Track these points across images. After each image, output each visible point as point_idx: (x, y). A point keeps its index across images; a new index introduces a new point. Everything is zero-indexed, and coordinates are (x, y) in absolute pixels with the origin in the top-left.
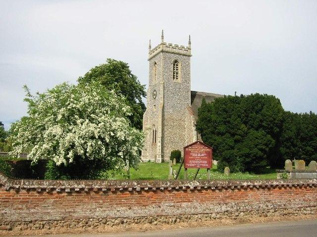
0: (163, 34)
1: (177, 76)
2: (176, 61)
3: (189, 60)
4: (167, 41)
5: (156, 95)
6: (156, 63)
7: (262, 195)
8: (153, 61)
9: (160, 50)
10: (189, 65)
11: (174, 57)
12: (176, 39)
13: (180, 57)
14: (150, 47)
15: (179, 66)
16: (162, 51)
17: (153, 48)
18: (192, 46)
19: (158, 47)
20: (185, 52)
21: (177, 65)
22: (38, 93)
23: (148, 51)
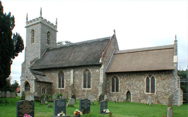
2: (48, 32)
8: (31, 28)
16: (41, 23)
19: (37, 19)
20: (54, 28)
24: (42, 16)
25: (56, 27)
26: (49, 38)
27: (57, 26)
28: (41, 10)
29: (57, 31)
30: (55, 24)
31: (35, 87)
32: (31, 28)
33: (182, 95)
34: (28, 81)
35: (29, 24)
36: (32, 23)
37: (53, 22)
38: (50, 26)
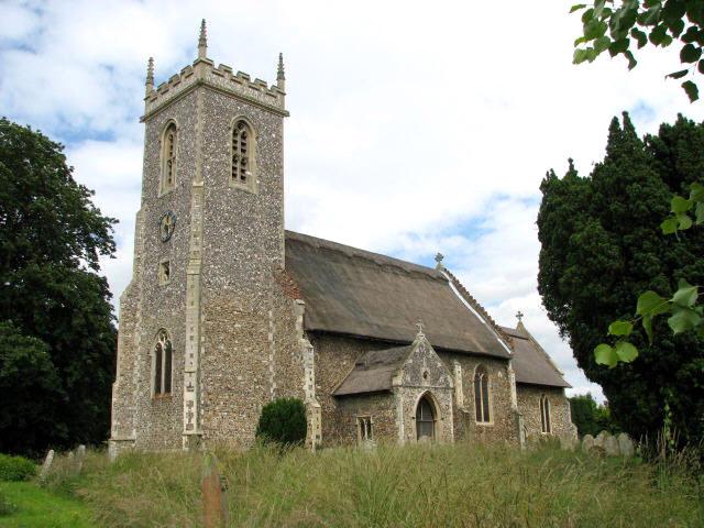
0: (203, 32)
1: (243, 171)
2: (241, 124)
3: (280, 124)
4: (217, 56)
5: (21, 478)
6: (172, 126)
7: (145, 372)
8: (162, 121)
9: (192, 80)
10: (278, 143)
11: (237, 111)
12: (244, 55)
13: (253, 111)
14: (150, 80)
15: (252, 142)
16: (200, 84)
17: (158, 83)
18: (288, 86)
19: (187, 72)
20: (269, 101)
21: (244, 137)
22: (520, 316)
23: (142, 92)
24: (210, 54)
25: (279, 92)
26: (243, 151)
27: (286, 91)
28: (281, 65)
29: (287, 114)
30: (272, 82)
31: (114, 380)
32: (162, 121)
33: (320, 423)
34: (433, 392)
35: (158, 103)
36: (168, 96)
37: (594, 167)
38: (267, 98)
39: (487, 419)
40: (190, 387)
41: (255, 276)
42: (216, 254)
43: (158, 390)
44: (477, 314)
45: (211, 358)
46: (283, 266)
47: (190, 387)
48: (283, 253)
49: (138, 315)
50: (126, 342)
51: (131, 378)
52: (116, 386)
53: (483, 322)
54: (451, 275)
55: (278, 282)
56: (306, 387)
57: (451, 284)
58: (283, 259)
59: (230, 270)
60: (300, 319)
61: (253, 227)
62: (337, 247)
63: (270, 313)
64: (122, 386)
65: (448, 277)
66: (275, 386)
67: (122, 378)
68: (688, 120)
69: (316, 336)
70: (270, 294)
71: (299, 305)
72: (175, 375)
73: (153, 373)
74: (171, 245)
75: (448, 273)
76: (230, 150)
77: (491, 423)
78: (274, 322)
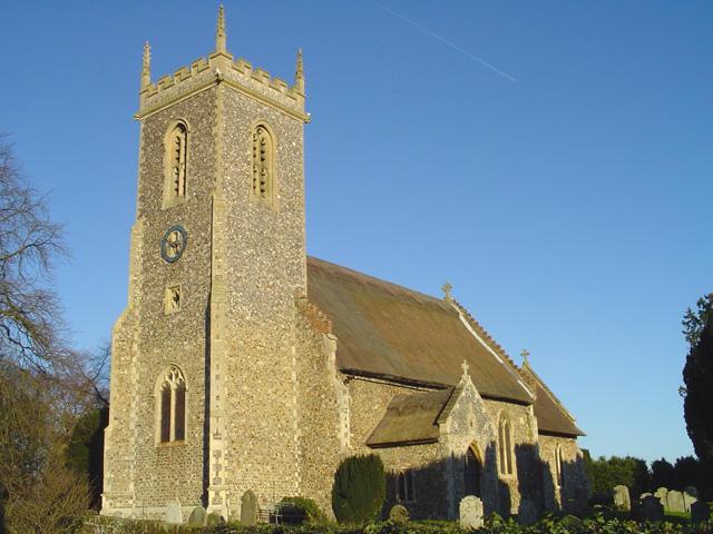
7: (146, 415)
39: (510, 472)
40: (217, 434)
41: (277, 306)
42: (239, 278)
43: (165, 437)
44: (493, 353)
45: (234, 400)
46: (305, 293)
47: (217, 434)
48: (305, 280)
49: (135, 347)
50: (121, 380)
51: (128, 423)
52: (108, 431)
53: (501, 361)
54: (461, 307)
55: (302, 313)
56: (340, 436)
57: (462, 318)
58: (305, 286)
59: (252, 298)
60: (333, 357)
61: (275, 249)
62: (370, 279)
63: (293, 348)
64: (117, 432)
65: (457, 309)
66: (299, 433)
67: (116, 422)
68: (673, 462)
69: (349, 373)
70: (293, 326)
71: (331, 343)
72: (191, 420)
73: (159, 417)
74: (181, 268)
75: (458, 304)
76: (250, 159)
77: (415, 501)
78: (298, 360)
